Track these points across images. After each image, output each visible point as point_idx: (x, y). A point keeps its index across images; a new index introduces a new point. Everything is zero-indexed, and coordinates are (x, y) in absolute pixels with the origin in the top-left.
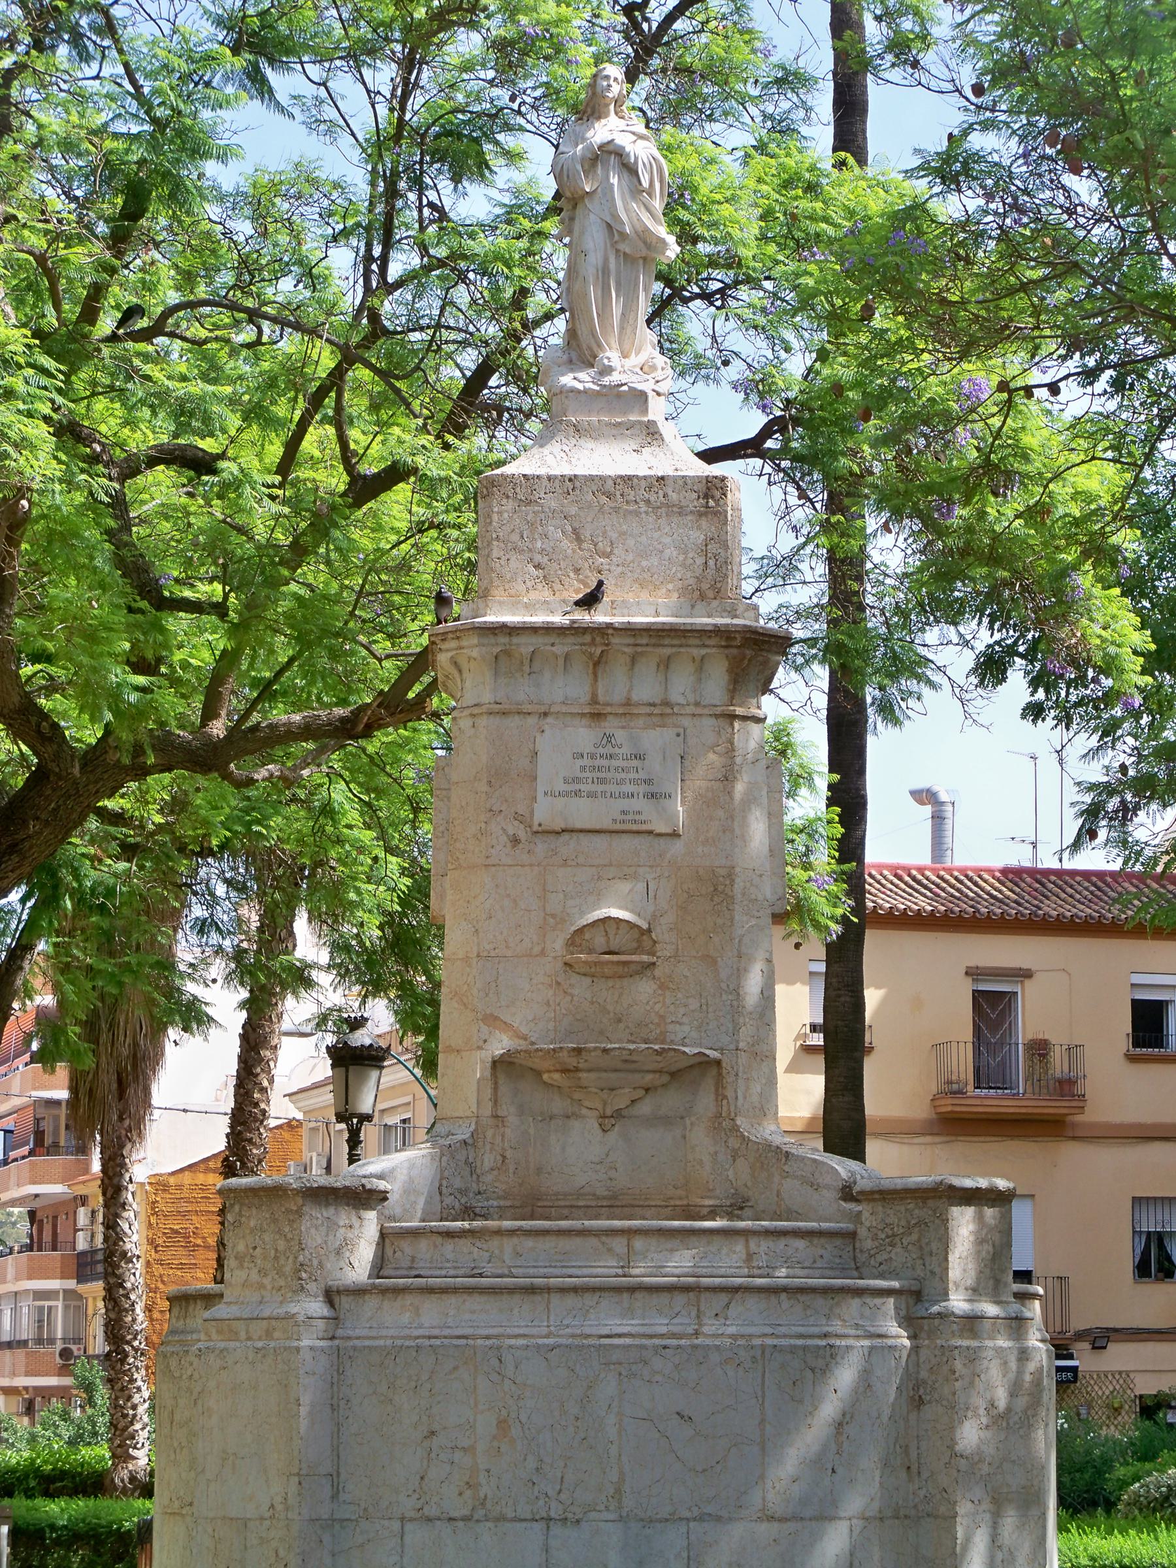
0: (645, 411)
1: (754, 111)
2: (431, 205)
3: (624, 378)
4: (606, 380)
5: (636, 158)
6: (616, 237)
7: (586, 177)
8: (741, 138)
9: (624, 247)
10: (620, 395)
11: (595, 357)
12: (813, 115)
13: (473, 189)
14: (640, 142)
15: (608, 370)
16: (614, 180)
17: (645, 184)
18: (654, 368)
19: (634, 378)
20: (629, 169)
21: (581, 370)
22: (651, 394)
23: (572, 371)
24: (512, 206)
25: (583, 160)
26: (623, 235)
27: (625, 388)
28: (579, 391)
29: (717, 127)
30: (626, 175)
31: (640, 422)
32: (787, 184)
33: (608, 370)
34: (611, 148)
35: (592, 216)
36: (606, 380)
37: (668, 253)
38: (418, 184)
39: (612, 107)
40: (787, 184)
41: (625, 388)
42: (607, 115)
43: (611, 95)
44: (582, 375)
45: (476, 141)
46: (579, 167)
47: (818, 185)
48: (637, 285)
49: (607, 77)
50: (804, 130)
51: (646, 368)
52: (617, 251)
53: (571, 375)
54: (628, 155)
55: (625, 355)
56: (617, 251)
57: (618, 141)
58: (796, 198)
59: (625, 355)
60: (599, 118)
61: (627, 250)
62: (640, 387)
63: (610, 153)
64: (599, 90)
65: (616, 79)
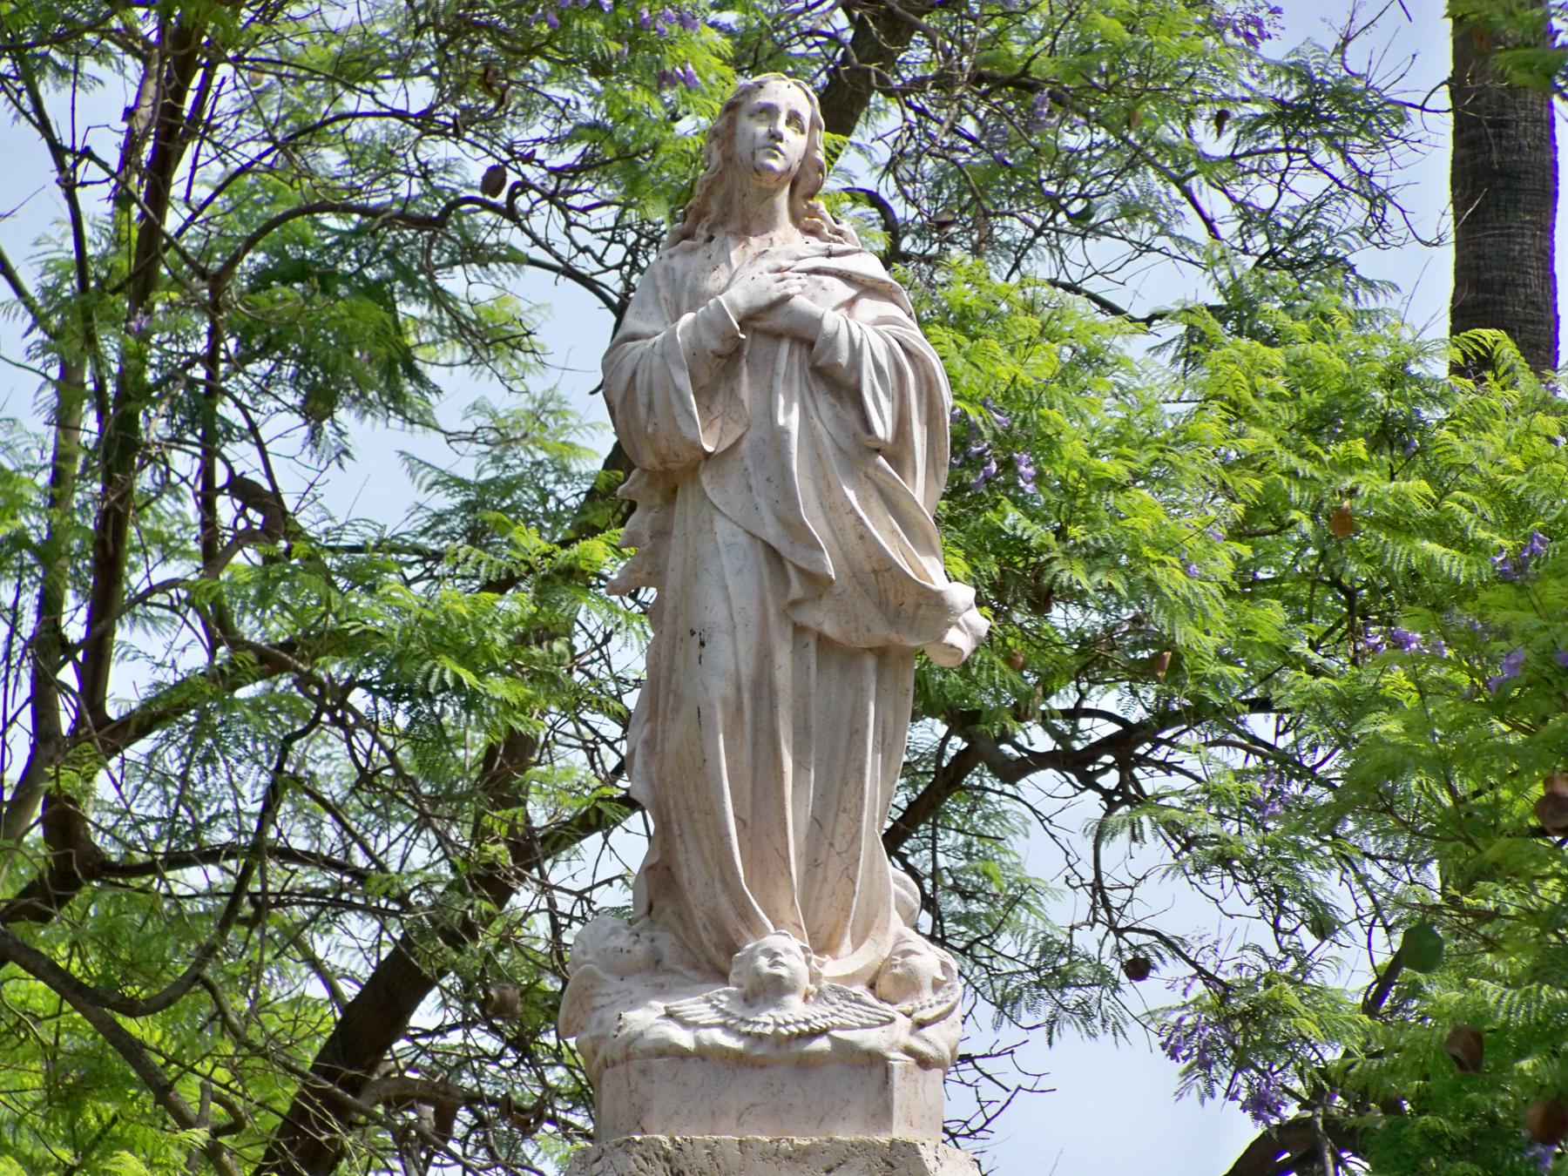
0: (883, 1114)
1: (1216, 203)
2: (240, 487)
3: (818, 1014)
4: (766, 1020)
5: (856, 353)
6: (796, 589)
7: (705, 408)
8: (1176, 283)
9: (824, 620)
10: (807, 1064)
11: (731, 948)
12: (1392, 214)
13: (365, 431)
14: (870, 308)
15: (772, 989)
16: (790, 419)
17: (883, 428)
18: (909, 984)
19: (850, 1014)
20: (835, 382)
21: (685, 986)
22: (899, 1060)
23: (660, 991)
24: (484, 487)
25: (695, 358)
26: (816, 582)
27: (822, 1044)
28: (681, 1054)
29: (1103, 250)
30: (824, 402)
31: (866, 1148)
32: (1320, 424)
33: (772, 989)
34: (778, 321)
35: (722, 528)
36: (766, 1020)
37: (954, 637)
38: (202, 422)
39: (782, 200)
40: (1320, 424)
41: (822, 1044)
42: (766, 224)
43: (777, 164)
44: (694, 1006)
45: (378, 293)
46: (683, 380)
47: (1413, 424)
48: (857, 732)
49: (770, 111)
50: (1367, 261)
51: (885, 985)
52: (799, 630)
53: (659, 1006)
54: (832, 341)
55: (822, 944)
56: (799, 630)
57: (801, 302)
58: (1349, 465)
59: (822, 944)
60: (744, 233)
61: (830, 629)
62: (872, 1039)
63: (777, 336)
64: (742, 148)
65: (794, 118)
